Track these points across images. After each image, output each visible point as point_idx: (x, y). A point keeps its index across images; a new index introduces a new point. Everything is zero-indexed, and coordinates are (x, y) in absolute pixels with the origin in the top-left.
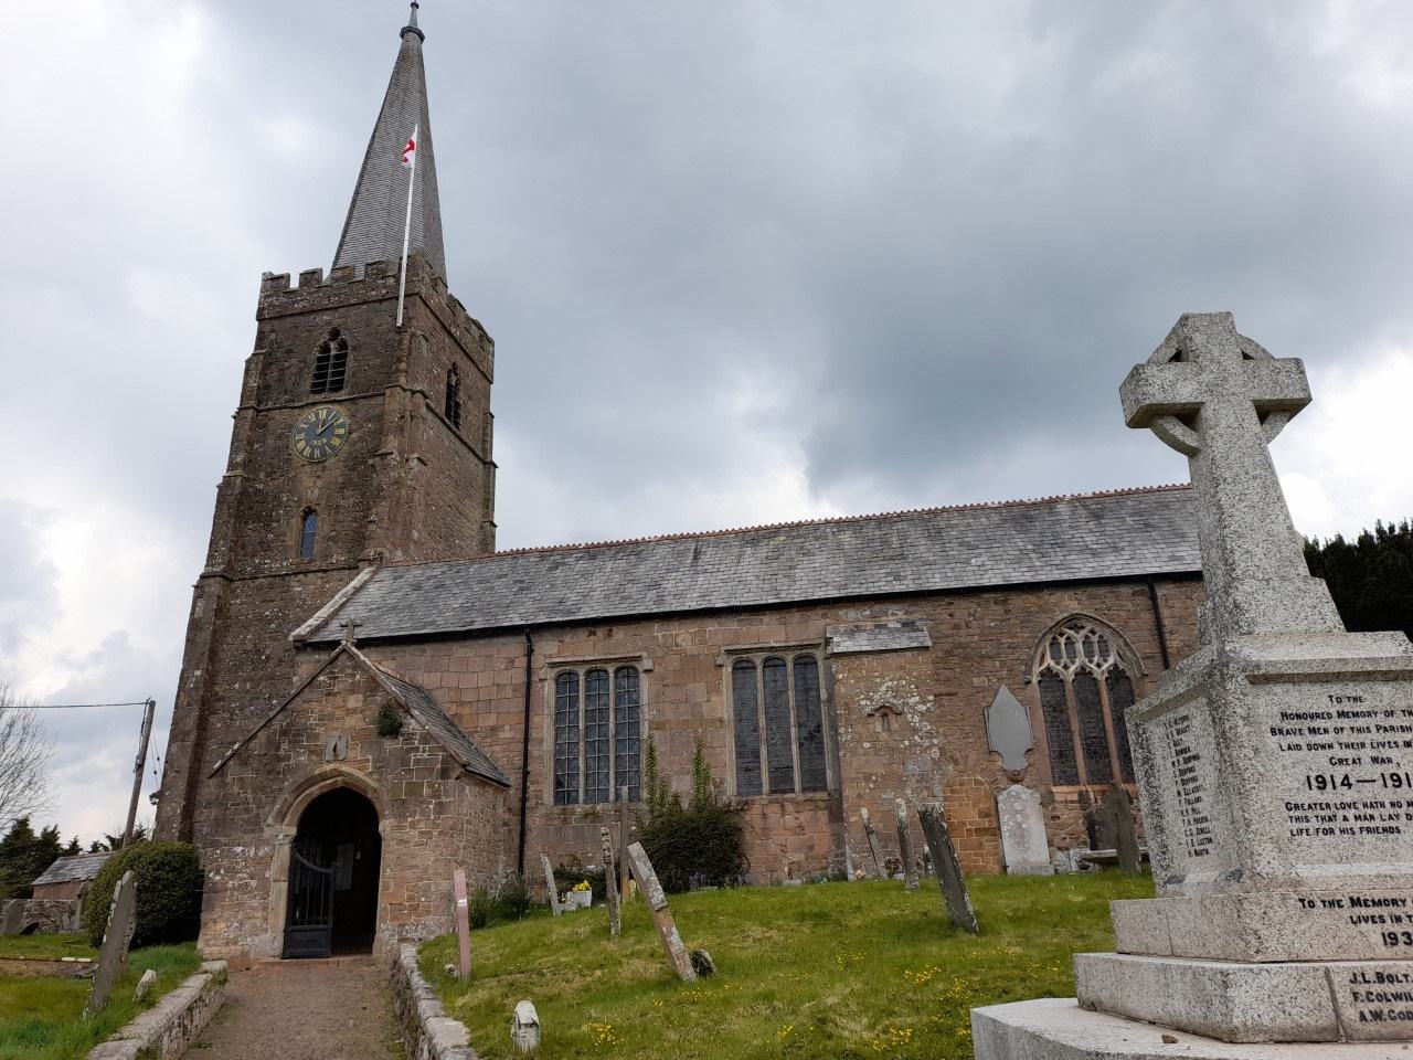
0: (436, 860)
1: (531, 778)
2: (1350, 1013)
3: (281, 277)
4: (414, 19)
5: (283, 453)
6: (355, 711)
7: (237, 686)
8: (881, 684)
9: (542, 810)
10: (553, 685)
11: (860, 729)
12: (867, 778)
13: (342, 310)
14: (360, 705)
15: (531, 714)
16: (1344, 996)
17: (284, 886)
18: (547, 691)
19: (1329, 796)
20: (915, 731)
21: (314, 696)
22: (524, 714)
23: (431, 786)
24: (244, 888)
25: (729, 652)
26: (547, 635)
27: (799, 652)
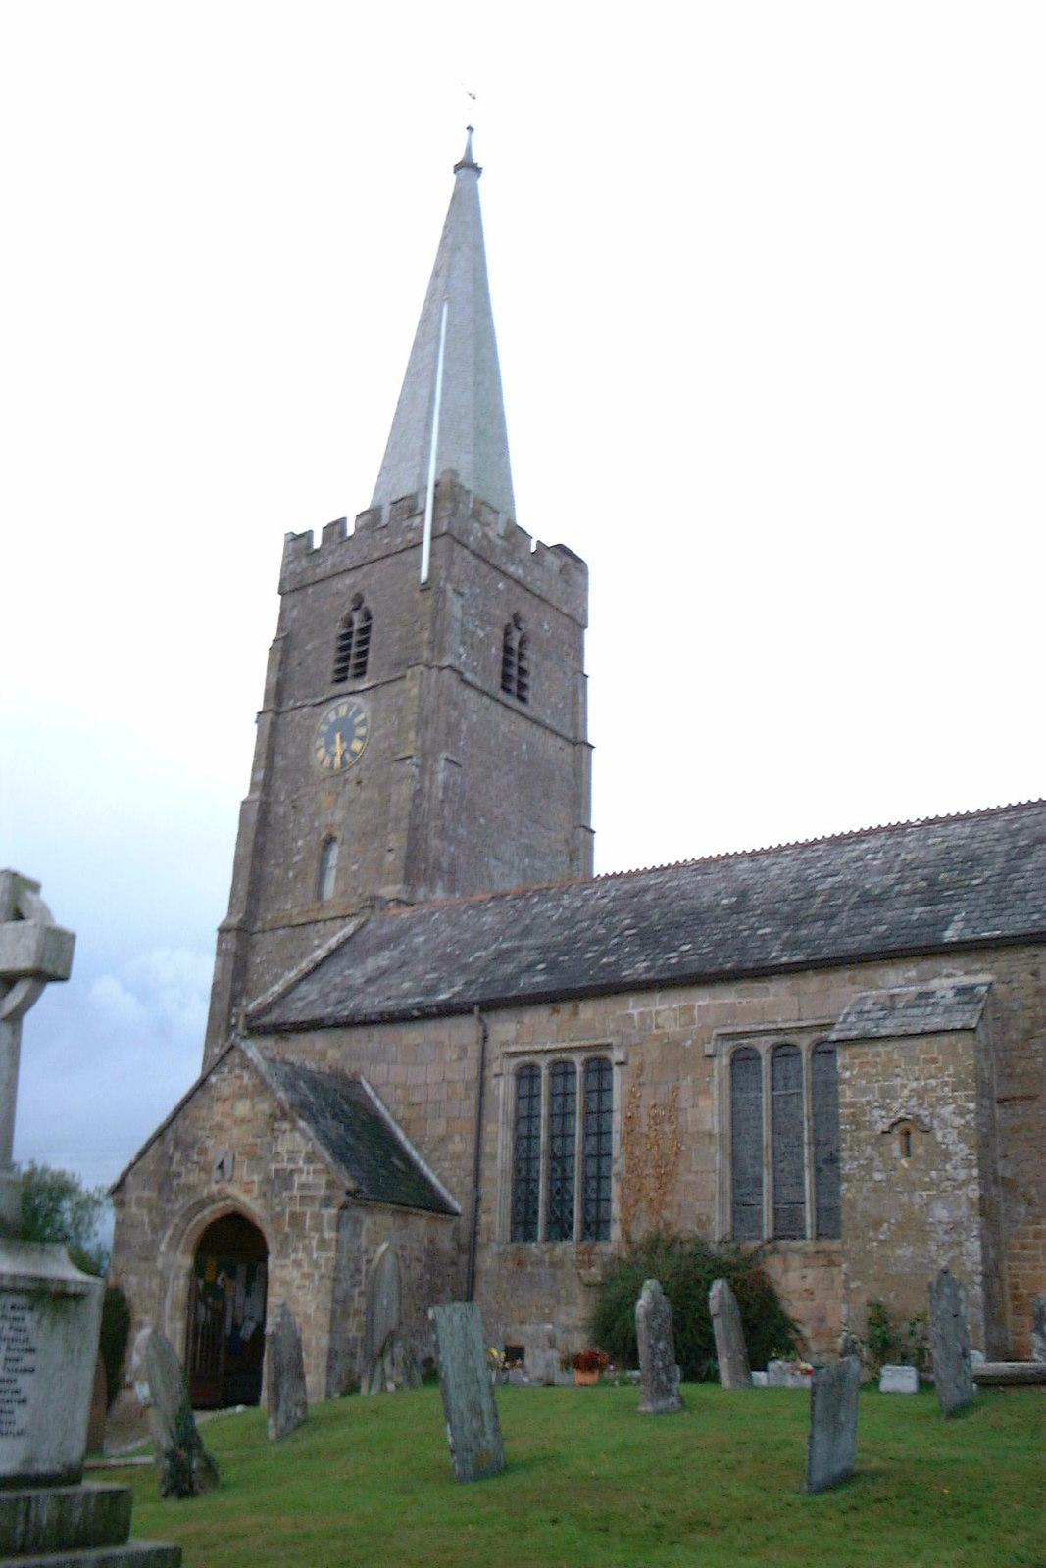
3: (302, 536)
4: (469, 150)
6: (243, 1121)
9: (495, 1248)
10: (512, 1081)
11: (869, 1150)
13: (365, 569)
15: (485, 1122)
18: (503, 1089)
25: (725, 1037)
26: (503, 1015)
27: (816, 1035)
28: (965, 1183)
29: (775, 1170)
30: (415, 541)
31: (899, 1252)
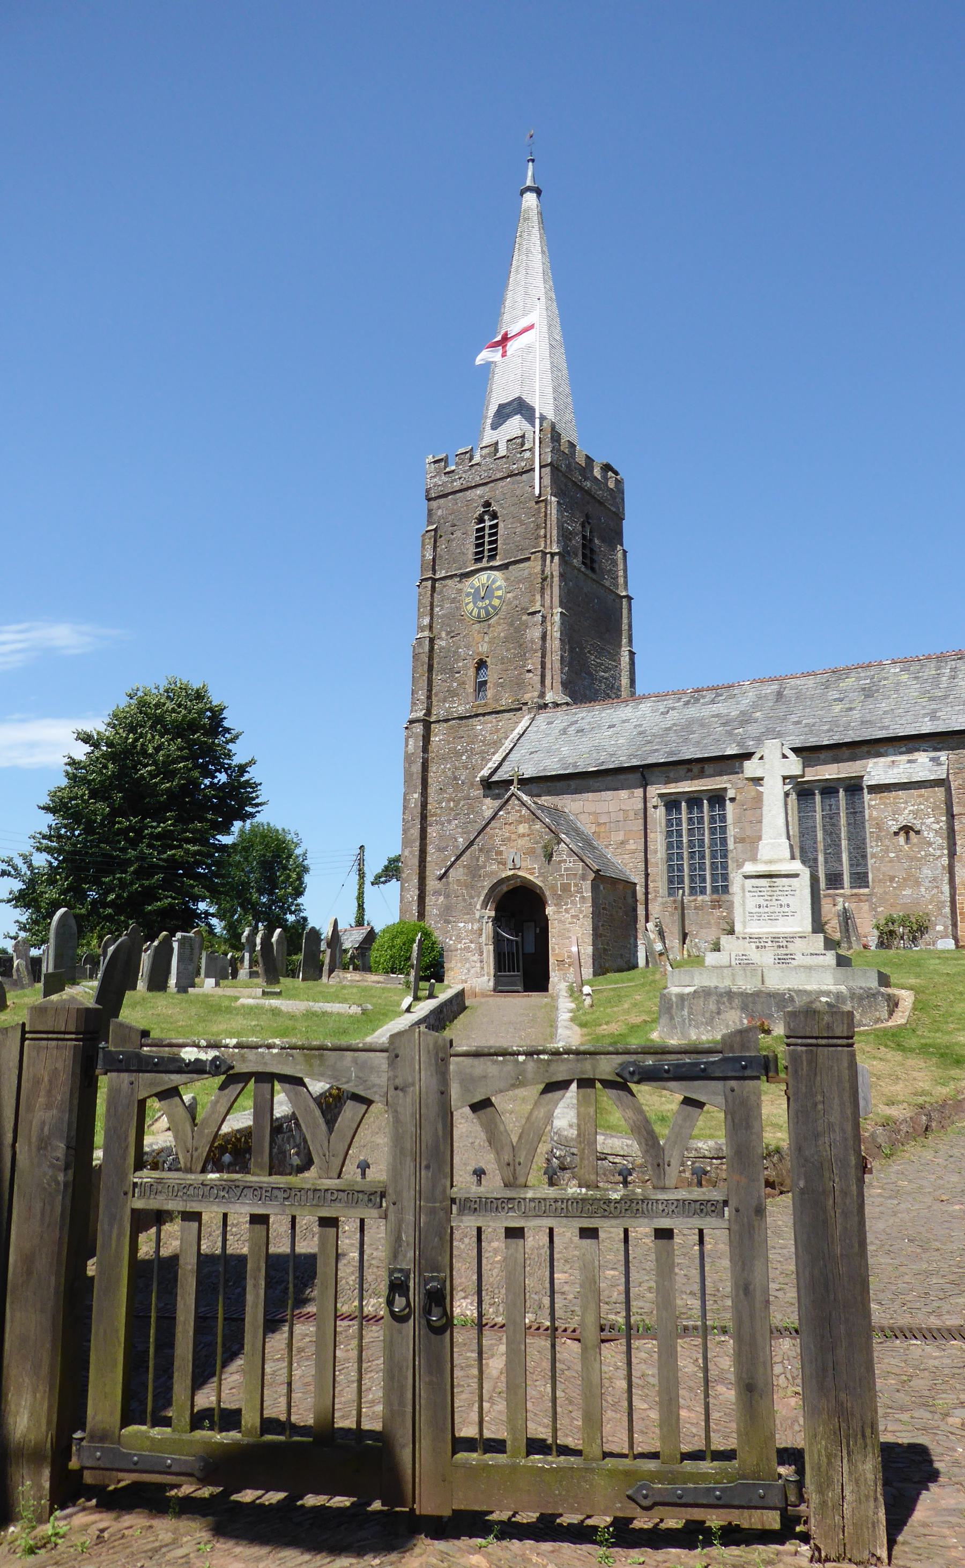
0: (583, 934)
1: (650, 878)
2: (733, 963)
5: (456, 616)
6: (524, 835)
7: (444, 804)
8: (905, 808)
11: (887, 842)
12: (892, 879)
14: (527, 831)
16: (733, 959)
17: (491, 948)
19: (761, 910)
20: (930, 844)
21: (498, 825)
22: (643, 832)
23: (576, 885)
24: (467, 949)
28: (940, 857)
29: (826, 854)
30: (528, 468)
31: (904, 893)
